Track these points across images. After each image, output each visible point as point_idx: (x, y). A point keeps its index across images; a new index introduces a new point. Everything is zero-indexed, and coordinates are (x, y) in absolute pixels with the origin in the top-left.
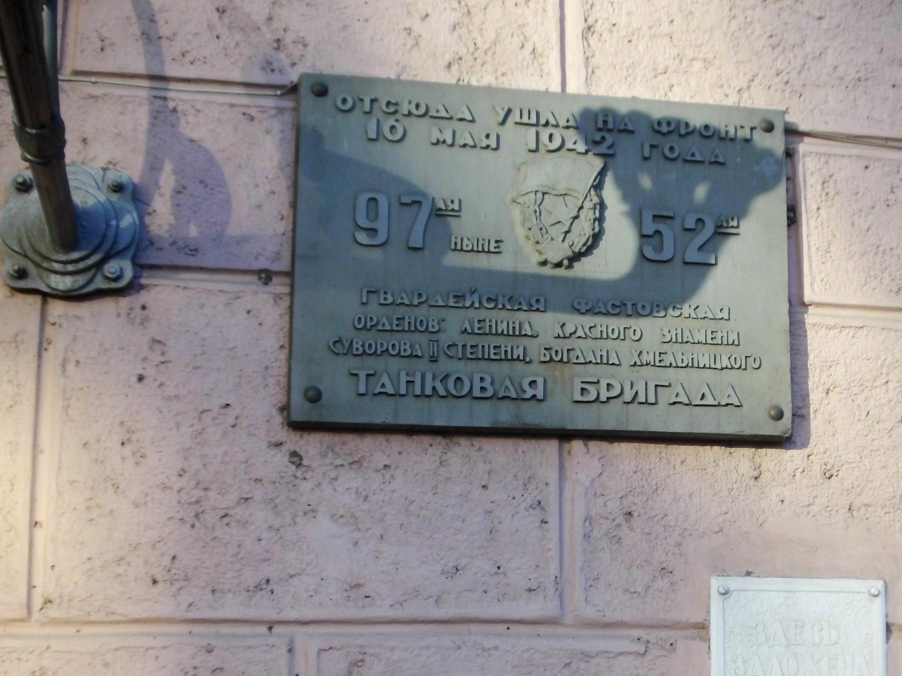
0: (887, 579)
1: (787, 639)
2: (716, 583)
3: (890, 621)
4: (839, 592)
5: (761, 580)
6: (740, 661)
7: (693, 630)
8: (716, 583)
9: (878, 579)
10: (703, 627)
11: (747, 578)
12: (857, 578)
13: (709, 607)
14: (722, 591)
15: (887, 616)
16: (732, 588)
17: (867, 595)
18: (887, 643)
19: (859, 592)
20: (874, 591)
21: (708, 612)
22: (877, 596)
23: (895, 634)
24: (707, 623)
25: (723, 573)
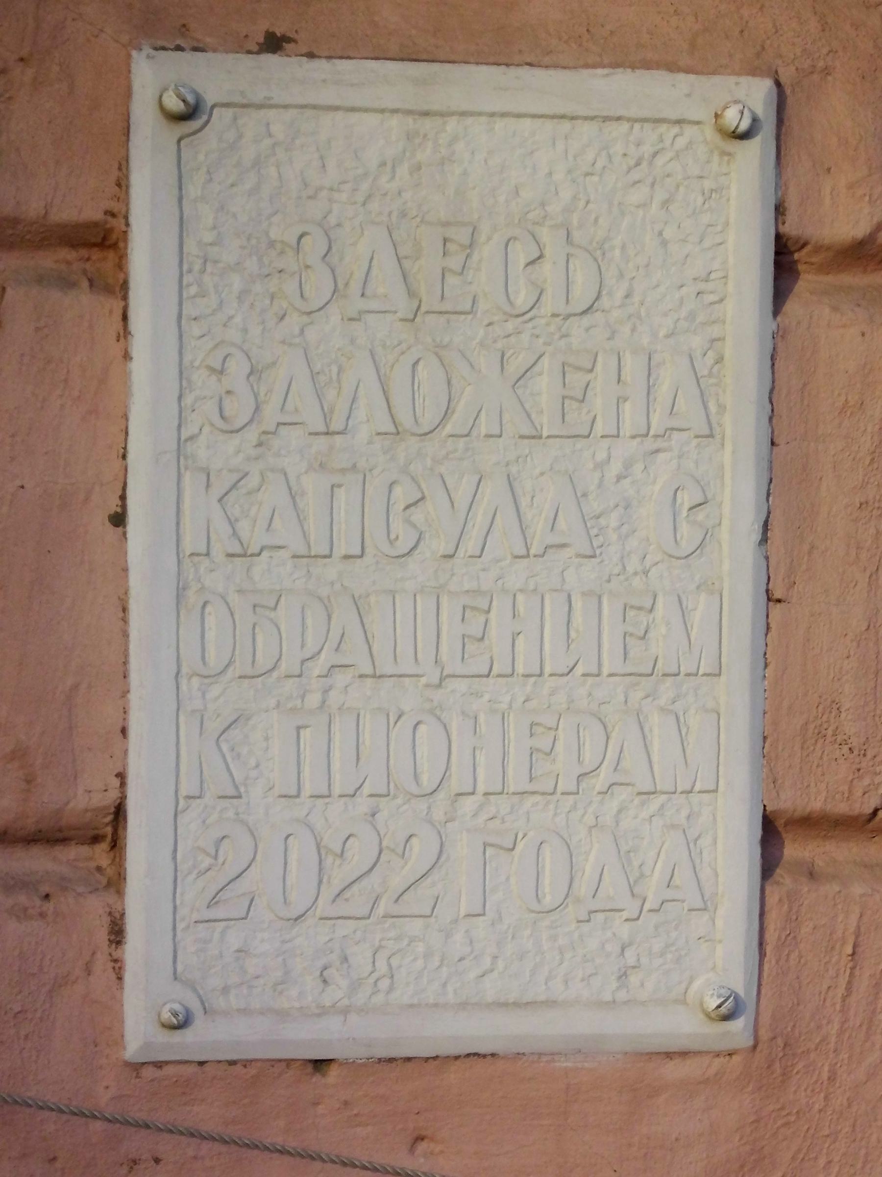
0: (787, 75)
1: (412, 293)
2: (152, 78)
3: (790, 228)
4: (606, 119)
5: (321, 67)
6: (238, 367)
7: (66, 253)
8: (152, 78)
9: (754, 72)
10: (100, 243)
11: (271, 60)
12: (672, 67)
13: (123, 165)
14: (173, 103)
15: (780, 210)
16: (210, 98)
17: (709, 132)
18: (776, 313)
19: (679, 122)
20: (731, 117)
21: (122, 184)
22: (745, 136)
23: (807, 282)
24: (117, 224)
25: (182, 38)
